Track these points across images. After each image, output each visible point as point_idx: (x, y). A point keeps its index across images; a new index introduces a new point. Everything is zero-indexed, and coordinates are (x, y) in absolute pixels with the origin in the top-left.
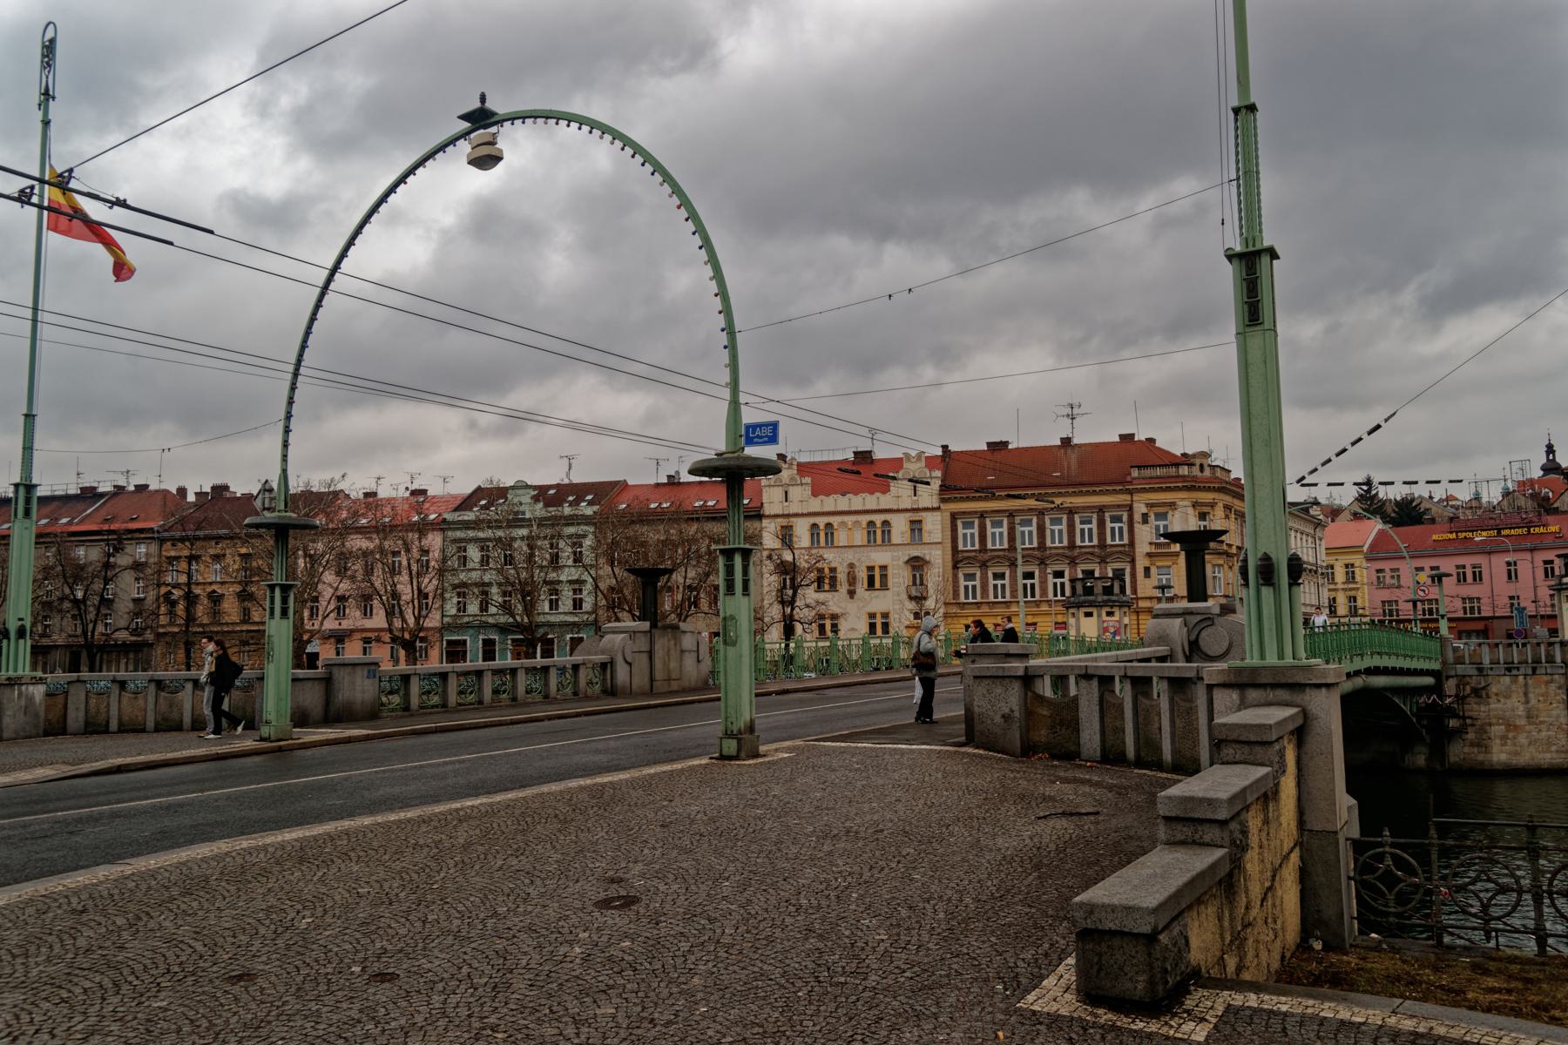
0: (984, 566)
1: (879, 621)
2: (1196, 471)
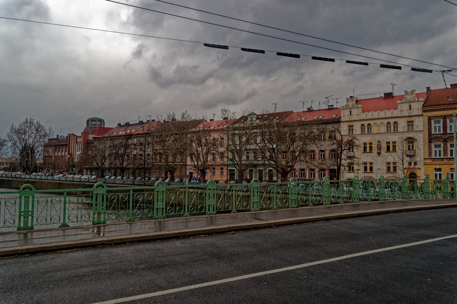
0: (445, 141)
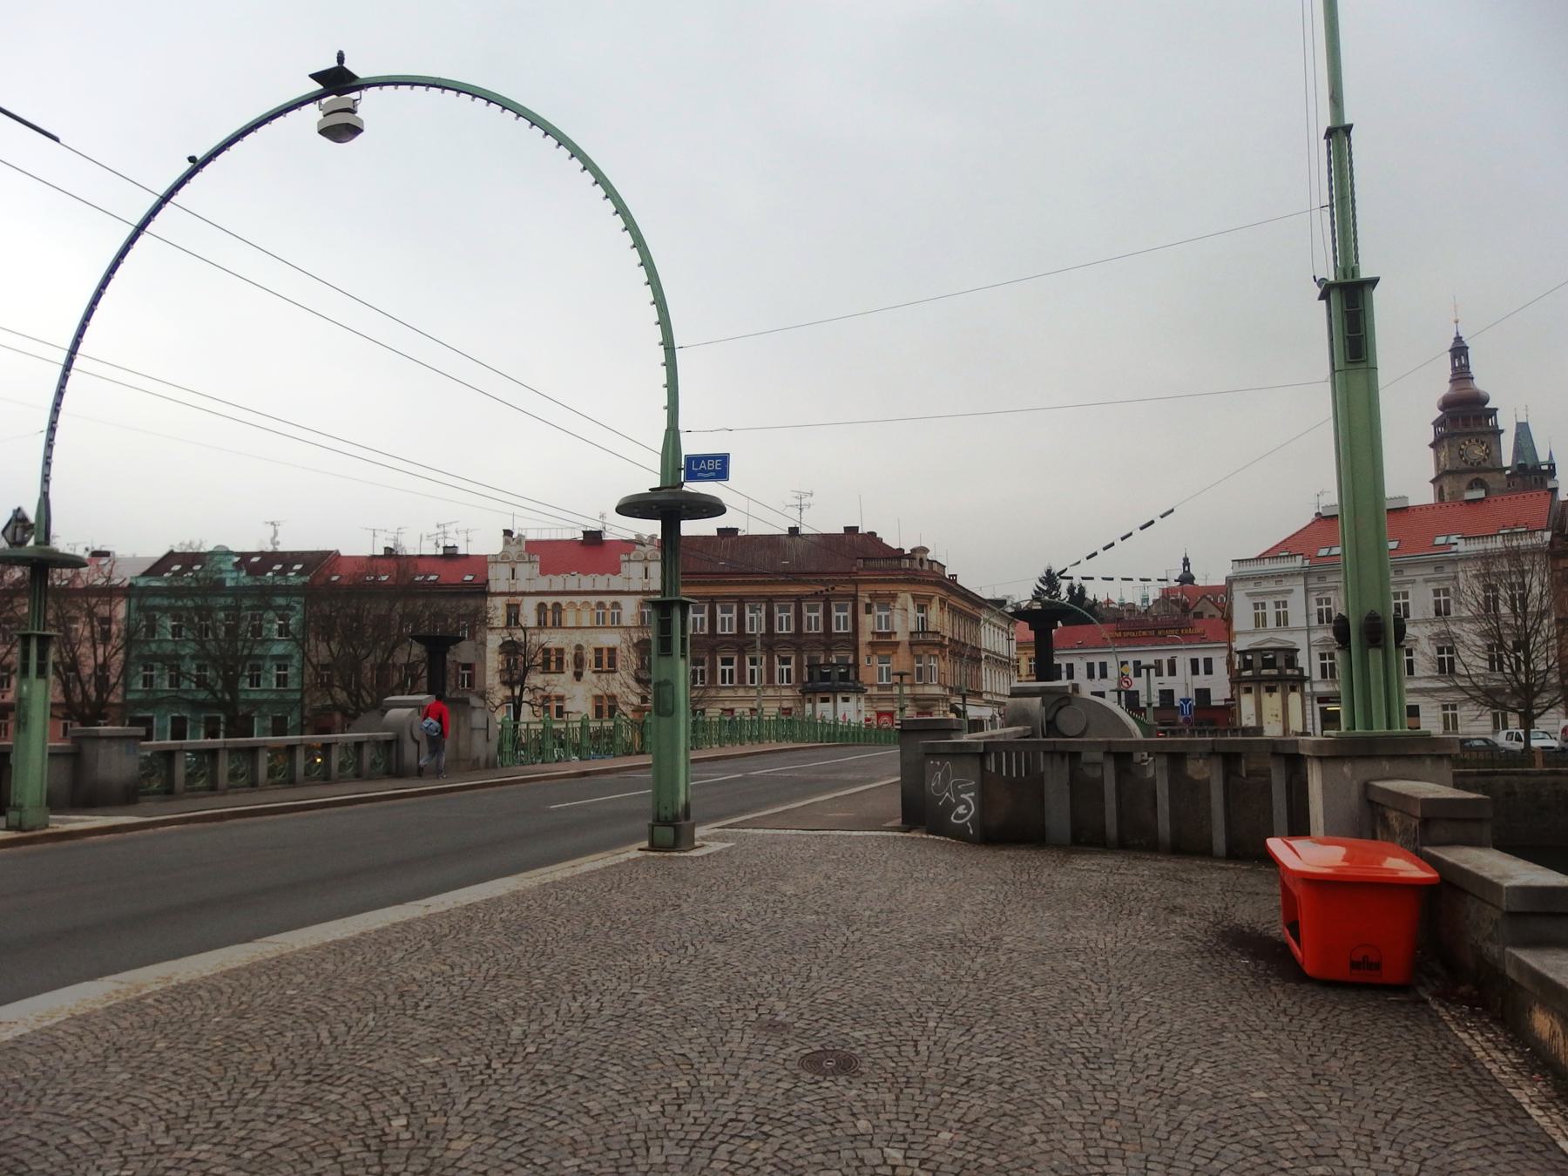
1: (606, 704)
2: (916, 565)
